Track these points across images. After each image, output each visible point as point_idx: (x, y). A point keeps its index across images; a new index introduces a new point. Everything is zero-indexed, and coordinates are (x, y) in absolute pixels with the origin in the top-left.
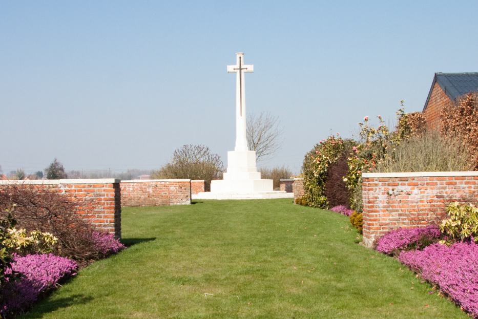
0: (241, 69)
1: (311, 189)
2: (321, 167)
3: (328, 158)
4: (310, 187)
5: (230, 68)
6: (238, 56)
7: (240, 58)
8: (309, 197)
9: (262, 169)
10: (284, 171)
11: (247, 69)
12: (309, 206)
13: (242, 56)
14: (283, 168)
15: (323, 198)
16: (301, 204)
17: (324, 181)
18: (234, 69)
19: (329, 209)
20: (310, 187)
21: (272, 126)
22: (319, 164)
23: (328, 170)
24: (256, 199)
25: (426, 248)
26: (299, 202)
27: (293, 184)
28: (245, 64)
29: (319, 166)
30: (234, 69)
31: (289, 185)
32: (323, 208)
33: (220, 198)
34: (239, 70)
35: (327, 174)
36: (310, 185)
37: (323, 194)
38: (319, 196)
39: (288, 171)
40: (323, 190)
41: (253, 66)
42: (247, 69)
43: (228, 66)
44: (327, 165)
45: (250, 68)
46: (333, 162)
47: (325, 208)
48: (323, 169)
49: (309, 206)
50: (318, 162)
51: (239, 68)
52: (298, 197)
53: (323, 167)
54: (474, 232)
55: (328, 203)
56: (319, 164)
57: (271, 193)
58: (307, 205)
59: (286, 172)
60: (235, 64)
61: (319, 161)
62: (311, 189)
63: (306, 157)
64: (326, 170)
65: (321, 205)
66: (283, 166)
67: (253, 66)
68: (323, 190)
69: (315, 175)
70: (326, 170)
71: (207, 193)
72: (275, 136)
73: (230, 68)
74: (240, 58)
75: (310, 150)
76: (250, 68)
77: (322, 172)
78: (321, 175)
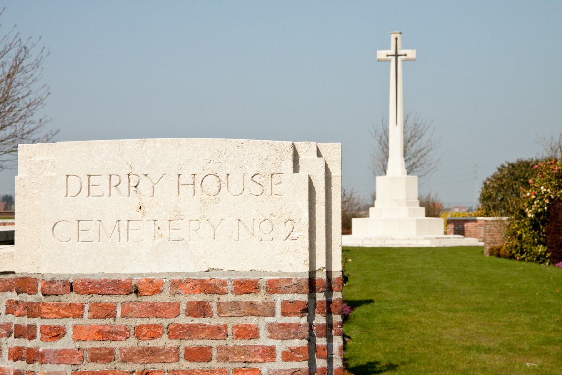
0: (397, 55)
1: (521, 235)
2: (537, 204)
3: (549, 190)
4: (519, 232)
5: (382, 54)
6: (393, 37)
7: (396, 39)
8: (517, 246)
9: (354, 196)
10: (431, 202)
11: (405, 55)
12: (516, 259)
13: (398, 36)
14: (429, 197)
15: (541, 249)
16: (499, 256)
17: (543, 224)
18: (388, 56)
19: (549, 264)
20: (519, 232)
21: (422, 135)
22: (534, 199)
23: (548, 209)
24: (421, 246)
25: (19, 362)
26: (496, 253)
27: (466, 225)
28: (403, 48)
29: (535, 203)
30: (388, 56)
31: (461, 226)
32: (541, 263)
33: (368, 244)
34: (394, 58)
35: (547, 213)
36: (518, 229)
37: (540, 242)
38: (535, 244)
39: (437, 202)
40: (540, 237)
41: (414, 51)
42: (405, 55)
43: (378, 52)
44: (547, 201)
45: (411, 54)
46: (556, 197)
47: (543, 262)
48: (541, 207)
49: (516, 259)
50: (533, 197)
51: (394, 53)
52: (492, 245)
53: (541, 203)
54: (350, 309)
55: (548, 255)
56: (534, 199)
57: (442, 238)
58: (512, 257)
59: (434, 204)
60: (389, 48)
61: (535, 195)
62: (521, 235)
63: (485, 183)
64: (546, 208)
65: (538, 259)
66: (429, 195)
67: (414, 51)
68: (540, 237)
69: (529, 215)
70: (546, 208)
71: (346, 237)
72: (428, 151)
73: (382, 54)
74: (396, 39)
75: (492, 174)
76: (411, 54)
77: (539, 210)
78: (537, 215)
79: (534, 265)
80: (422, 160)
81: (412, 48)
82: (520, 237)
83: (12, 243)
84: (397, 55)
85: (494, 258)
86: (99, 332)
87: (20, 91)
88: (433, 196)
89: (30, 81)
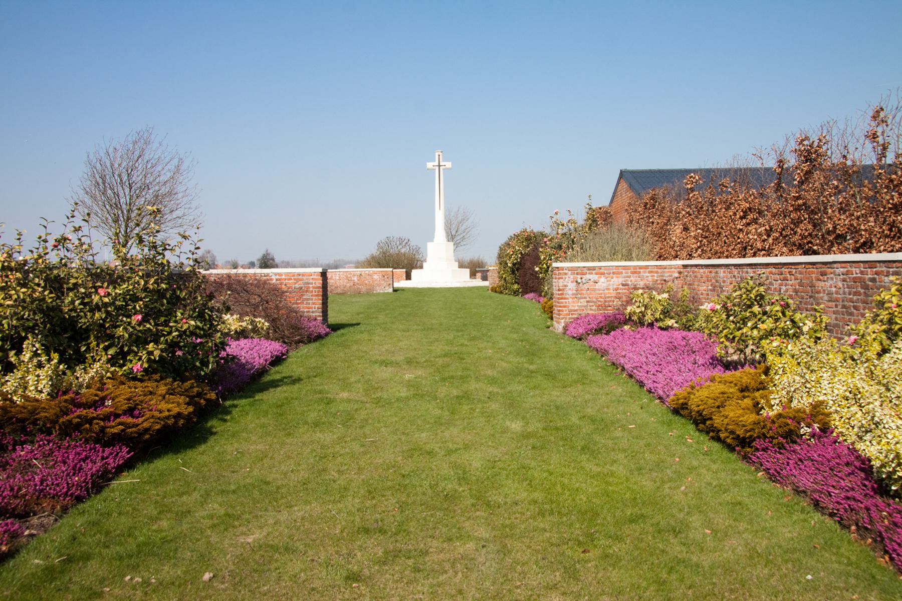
6: (437, 154)
13: (440, 154)
15: (516, 286)
16: (496, 292)
17: (517, 270)
26: (494, 290)
28: (443, 161)
33: (420, 286)
35: (520, 263)
37: (516, 282)
38: (513, 284)
45: (449, 165)
55: (520, 290)
58: (501, 293)
60: (434, 161)
63: (500, 247)
65: (515, 293)
73: (430, 165)
76: (449, 165)
78: (514, 264)
79: (511, 297)
80: (468, 235)
81: (449, 161)
82: (505, 279)
83: (407, 279)
84: (439, 166)
85: (494, 294)
86: (683, 265)
87: (180, 188)
88: (481, 257)
89: (186, 180)
